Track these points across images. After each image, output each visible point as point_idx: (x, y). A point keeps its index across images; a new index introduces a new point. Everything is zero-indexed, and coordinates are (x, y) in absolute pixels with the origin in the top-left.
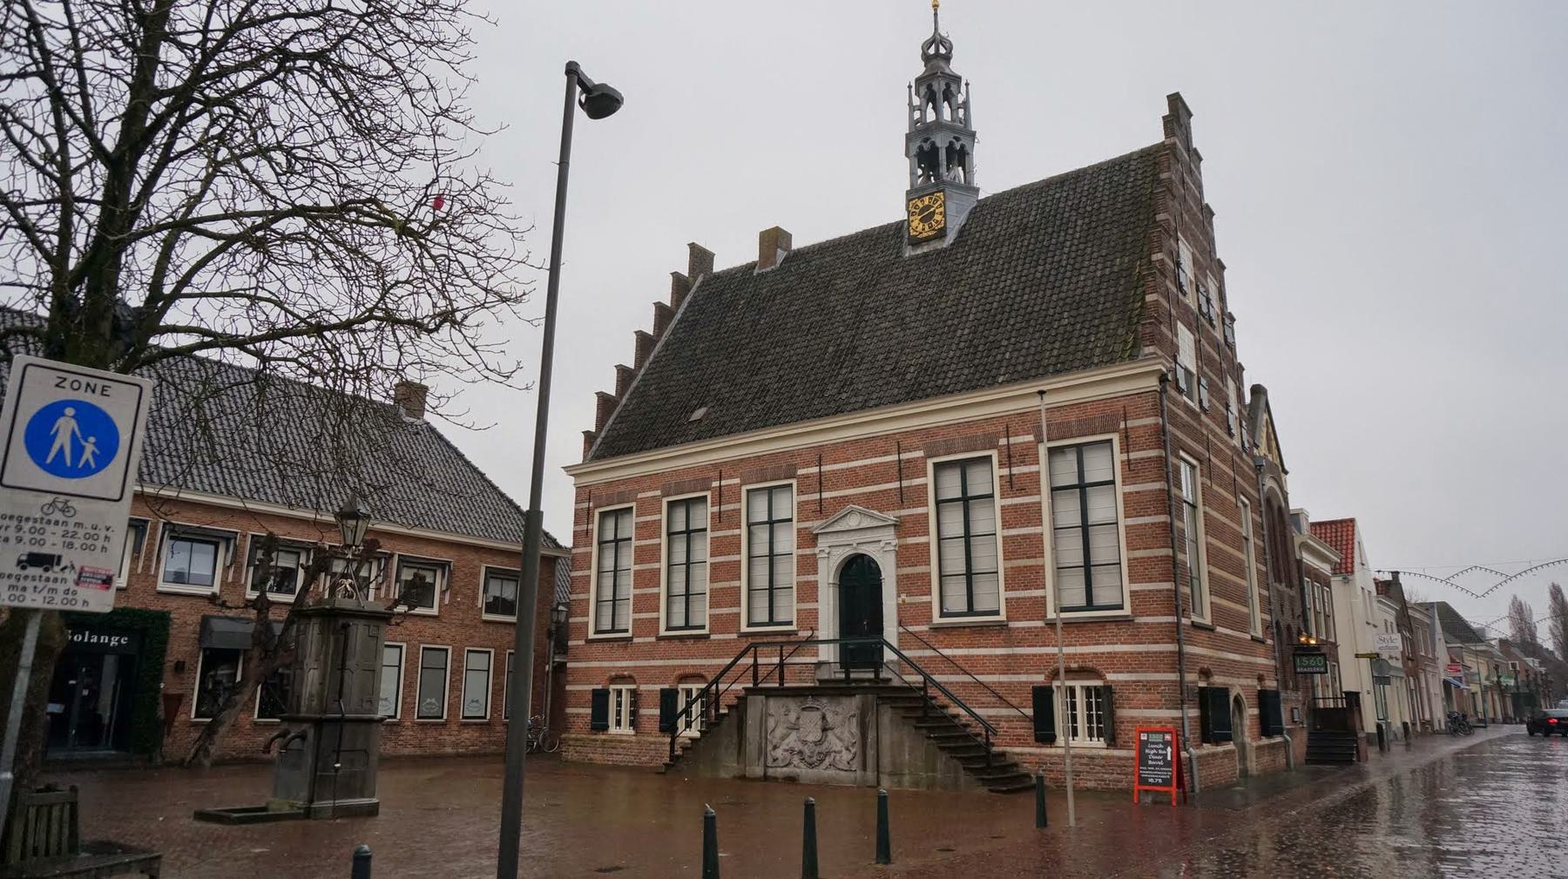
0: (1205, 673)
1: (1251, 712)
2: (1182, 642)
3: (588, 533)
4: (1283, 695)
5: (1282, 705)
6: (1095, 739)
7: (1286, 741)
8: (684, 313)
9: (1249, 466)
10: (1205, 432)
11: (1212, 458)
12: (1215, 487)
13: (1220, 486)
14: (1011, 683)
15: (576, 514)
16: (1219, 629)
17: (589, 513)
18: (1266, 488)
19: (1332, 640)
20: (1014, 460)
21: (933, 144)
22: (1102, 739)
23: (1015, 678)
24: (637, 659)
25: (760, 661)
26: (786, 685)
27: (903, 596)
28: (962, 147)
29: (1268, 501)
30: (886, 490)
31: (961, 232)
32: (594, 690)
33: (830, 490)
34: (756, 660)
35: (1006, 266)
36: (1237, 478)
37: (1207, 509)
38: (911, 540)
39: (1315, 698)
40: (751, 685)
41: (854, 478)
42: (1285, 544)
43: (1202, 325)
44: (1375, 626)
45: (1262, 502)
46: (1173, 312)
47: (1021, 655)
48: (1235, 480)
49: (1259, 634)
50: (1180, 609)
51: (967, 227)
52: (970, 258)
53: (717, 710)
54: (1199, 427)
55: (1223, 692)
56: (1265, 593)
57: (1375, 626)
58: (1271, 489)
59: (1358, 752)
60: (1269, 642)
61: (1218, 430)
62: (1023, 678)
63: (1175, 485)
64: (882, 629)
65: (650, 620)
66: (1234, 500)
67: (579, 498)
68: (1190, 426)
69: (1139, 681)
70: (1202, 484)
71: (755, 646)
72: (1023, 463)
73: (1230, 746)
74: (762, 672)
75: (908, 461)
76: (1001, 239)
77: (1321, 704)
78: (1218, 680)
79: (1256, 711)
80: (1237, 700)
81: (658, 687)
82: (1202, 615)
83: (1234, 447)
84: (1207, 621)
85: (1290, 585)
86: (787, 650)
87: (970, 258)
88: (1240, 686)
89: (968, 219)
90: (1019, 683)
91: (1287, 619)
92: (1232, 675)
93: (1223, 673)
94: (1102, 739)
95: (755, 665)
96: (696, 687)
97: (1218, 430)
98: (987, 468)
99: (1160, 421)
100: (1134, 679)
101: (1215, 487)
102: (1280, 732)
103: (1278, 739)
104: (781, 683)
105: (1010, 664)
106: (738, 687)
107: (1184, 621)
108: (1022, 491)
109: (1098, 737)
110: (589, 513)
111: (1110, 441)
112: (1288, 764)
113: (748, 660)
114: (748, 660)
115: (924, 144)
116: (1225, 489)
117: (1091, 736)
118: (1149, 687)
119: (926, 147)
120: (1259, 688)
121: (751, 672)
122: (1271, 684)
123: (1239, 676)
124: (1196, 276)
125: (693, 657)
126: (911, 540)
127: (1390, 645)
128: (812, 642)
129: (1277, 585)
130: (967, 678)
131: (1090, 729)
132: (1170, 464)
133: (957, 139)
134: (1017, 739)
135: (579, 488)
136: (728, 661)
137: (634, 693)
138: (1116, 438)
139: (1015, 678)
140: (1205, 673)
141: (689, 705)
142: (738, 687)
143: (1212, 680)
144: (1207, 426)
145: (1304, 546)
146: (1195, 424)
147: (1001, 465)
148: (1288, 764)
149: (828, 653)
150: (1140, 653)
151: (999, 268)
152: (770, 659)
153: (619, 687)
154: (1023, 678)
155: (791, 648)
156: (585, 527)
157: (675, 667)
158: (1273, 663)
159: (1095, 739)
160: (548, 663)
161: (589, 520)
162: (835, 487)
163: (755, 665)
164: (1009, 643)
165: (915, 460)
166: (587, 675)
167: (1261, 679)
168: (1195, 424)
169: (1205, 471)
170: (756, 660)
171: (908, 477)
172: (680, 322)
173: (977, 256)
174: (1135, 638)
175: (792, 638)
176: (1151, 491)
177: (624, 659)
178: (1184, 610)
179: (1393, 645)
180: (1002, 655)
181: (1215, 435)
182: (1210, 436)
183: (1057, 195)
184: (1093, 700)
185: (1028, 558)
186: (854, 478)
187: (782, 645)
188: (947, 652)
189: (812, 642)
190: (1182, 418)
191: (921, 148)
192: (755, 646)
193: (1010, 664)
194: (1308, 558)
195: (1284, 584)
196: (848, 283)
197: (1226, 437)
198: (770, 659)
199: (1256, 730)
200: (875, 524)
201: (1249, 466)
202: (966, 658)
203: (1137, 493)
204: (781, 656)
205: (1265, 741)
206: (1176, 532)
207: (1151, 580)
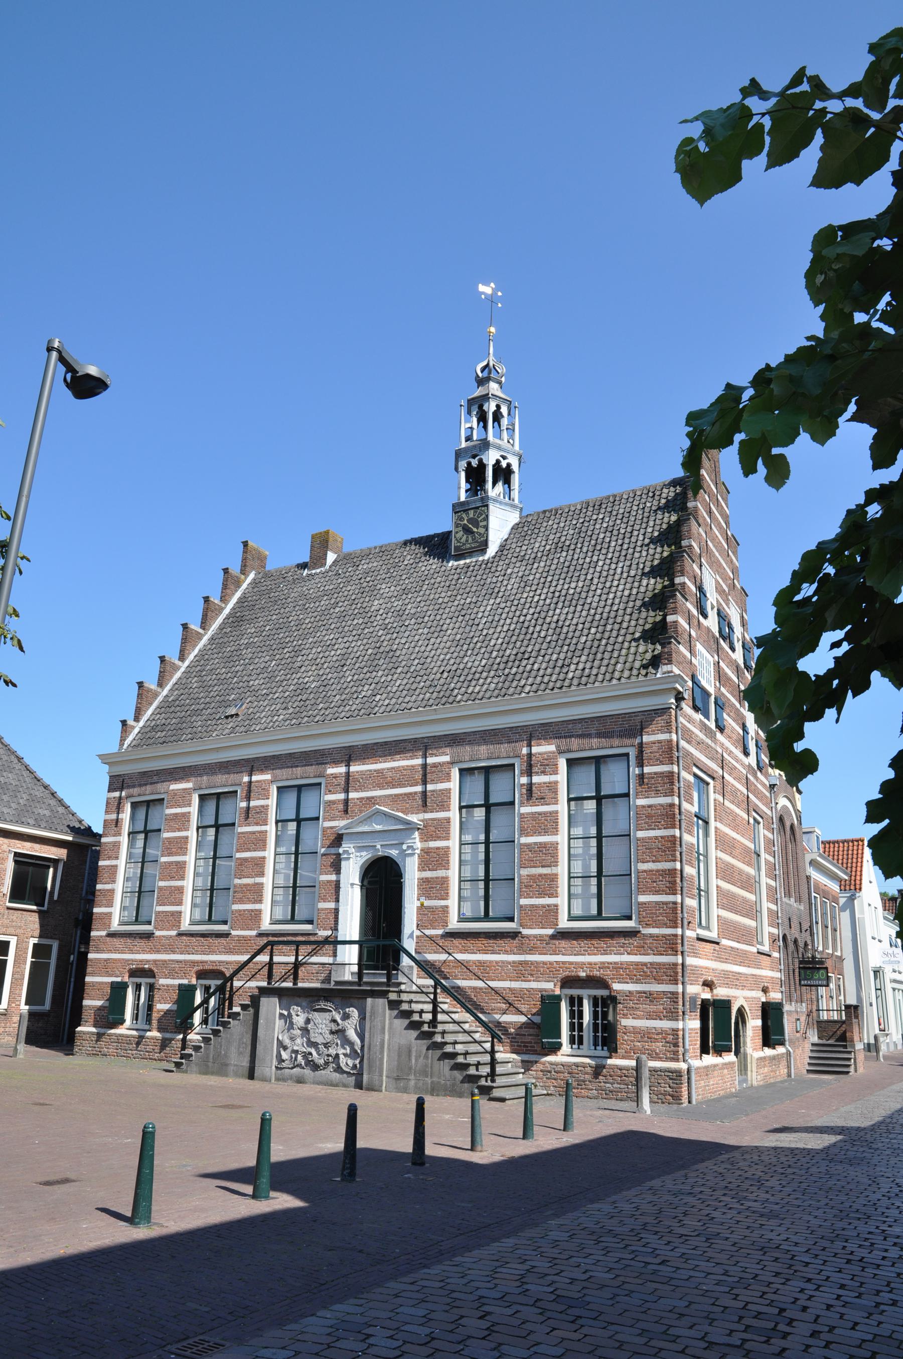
0: (708, 984)
1: (754, 1023)
2: (686, 953)
3: (117, 822)
4: (787, 1008)
5: (785, 1016)
6: (599, 1048)
7: (788, 1053)
8: (233, 608)
9: (764, 785)
10: (720, 750)
11: (726, 775)
12: (727, 803)
13: (733, 802)
14: (521, 990)
15: (108, 803)
16: (725, 942)
17: (119, 803)
18: (779, 806)
19: (838, 954)
20: (535, 769)
21: (481, 461)
22: (605, 1048)
23: (525, 985)
24: (158, 952)
25: (276, 959)
26: (300, 985)
27: (422, 899)
28: (509, 465)
29: (781, 819)
30: (411, 794)
31: (502, 547)
32: (112, 983)
33: (356, 790)
34: (271, 959)
35: (542, 580)
36: (751, 796)
37: (719, 825)
38: (433, 844)
39: (818, 1010)
40: (264, 984)
41: (379, 778)
42: (796, 858)
43: (723, 649)
44: (880, 941)
45: (774, 821)
46: (693, 633)
47: (532, 963)
48: (748, 797)
49: (766, 948)
50: (686, 923)
51: (509, 542)
52: (509, 571)
53: (230, 1008)
54: (713, 745)
55: (724, 1006)
56: (774, 907)
57: (880, 941)
58: (785, 807)
59: (855, 1062)
60: (776, 955)
61: (732, 748)
62: (534, 985)
63: (687, 801)
64: (892, 877)
65: (173, 914)
66: (745, 816)
67: (112, 787)
68: (708, 746)
69: (645, 992)
70: (715, 800)
71: (272, 944)
72: (544, 773)
73: (730, 1057)
74: (278, 972)
75: (435, 765)
76: (539, 555)
77: (824, 1016)
78: (721, 992)
79: (759, 1023)
80: (741, 1012)
81: (177, 982)
82: (708, 928)
83: (750, 765)
84: (713, 935)
85: (799, 900)
86: (304, 949)
87: (509, 571)
88: (744, 998)
89: (510, 534)
90: (528, 990)
91: (794, 933)
92: (736, 987)
93: (728, 985)
94: (605, 1048)
95: (271, 964)
96: (214, 983)
97: (732, 748)
98: (510, 775)
99: (674, 737)
100: (638, 989)
101: (727, 803)
102: (782, 1043)
103: (781, 1050)
104: (295, 984)
105: (522, 971)
106: (253, 984)
107: (689, 933)
108: (542, 800)
109: (603, 1046)
110: (119, 803)
111: (627, 755)
112: (789, 1075)
113: (264, 958)
114: (264, 958)
115: (472, 460)
116: (738, 806)
117: (596, 1045)
118: (650, 997)
119: (475, 463)
120: (764, 1000)
121: (265, 971)
122: (775, 996)
123: (744, 987)
124: (718, 601)
125: (212, 952)
126: (433, 844)
127: (893, 959)
128: (333, 943)
129: (785, 900)
130: (479, 984)
131: (596, 1038)
132: (681, 780)
133: (504, 458)
134: (525, 1046)
135: (112, 777)
136: (245, 958)
137: (151, 987)
138: (633, 753)
139: (525, 985)
140: (708, 984)
141: (205, 1001)
142: (253, 984)
143: (715, 991)
144: (722, 745)
145: (813, 863)
146: (709, 742)
147: (522, 774)
148: (789, 1075)
149: (350, 955)
150: (645, 964)
151: (536, 582)
152: (284, 958)
153: (138, 980)
154: (534, 985)
155: (309, 948)
156: (114, 816)
157: (194, 963)
158: (778, 975)
159: (599, 1048)
160: (73, 954)
161: (119, 809)
162: (361, 789)
163: (271, 964)
164: (521, 950)
165: (441, 764)
166: (107, 967)
167: (765, 990)
168: (709, 742)
169: (719, 787)
170: (271, 959)
171: (433, 782)
172: (227, 618)
173: (516, 570)
174: (641, 950)
175: (312, 939)
176: (661, 805)
177: (144, 952)
178: (689, 923)
179: (895, 959)
180: (514, 962)
181: (730, 753)
182: (725, 755)
183: (595, 517)
184: (599, 1009)
185: (543, 866)
186: (379, 778)
187: (298, 944)
188: (460, 957)
189: (333, 943)
190: (697, 736)
191: (469, 464)
192: (272, 944)
193: (522, 971)
194: (815, 875)
195: (793, 900)
196: (393, 588)
197: (741, 756)
198: (284, 958)
199: (760, 1041)
200: (401, 827)
201: (764, 785)
202: (481, 963)
203: (649, 806)
204: (297, 956)
205: (768, 1052)
206: (684, 846)
207: (657, 892)
